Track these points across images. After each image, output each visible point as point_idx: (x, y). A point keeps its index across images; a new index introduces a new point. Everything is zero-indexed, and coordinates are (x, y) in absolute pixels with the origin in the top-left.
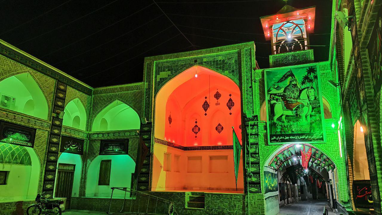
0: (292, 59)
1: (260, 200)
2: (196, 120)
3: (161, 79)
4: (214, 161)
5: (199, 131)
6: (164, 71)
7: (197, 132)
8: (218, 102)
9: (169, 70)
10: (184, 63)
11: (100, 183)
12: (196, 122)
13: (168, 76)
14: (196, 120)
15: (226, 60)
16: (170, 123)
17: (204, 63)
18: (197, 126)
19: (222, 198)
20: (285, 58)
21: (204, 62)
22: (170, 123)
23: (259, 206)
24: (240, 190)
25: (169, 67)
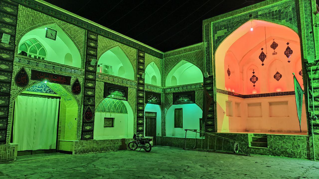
3: (218, 37)
4: (274, 107)
15: (282, 10)
16: (229, 75)
17: (259, 16)
18: (255, 76)
22: (229, 75)
25: (225, 25)
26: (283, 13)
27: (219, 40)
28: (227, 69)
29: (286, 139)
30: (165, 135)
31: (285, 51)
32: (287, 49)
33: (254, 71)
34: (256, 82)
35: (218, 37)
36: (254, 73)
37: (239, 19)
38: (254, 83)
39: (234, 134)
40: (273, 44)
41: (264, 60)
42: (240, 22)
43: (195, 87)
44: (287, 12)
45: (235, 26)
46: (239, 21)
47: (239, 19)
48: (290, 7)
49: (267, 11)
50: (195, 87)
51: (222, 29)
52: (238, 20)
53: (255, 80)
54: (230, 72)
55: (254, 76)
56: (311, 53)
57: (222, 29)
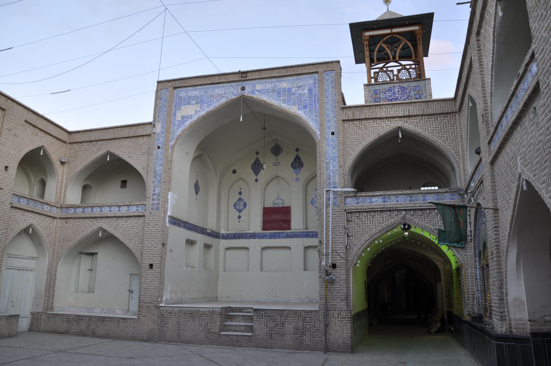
0: (398, 91)
1: (345, 318)
2: (240, 189)
3: (183, 117)
4: (267, 253)
5: (245, 208)
6: (189, 104)
7: (240, 210)
8: (277, 160)
9: (197, 103)
10: (224, 91)
11: (94, 293)
12: (240, 193)
13: (196, 113)
14: (240, 189)
15: (294, 89)
16: (197, 193)
17: (257, 92)
18: (243, 200)
19: (130, 233)
20: (388, 90)
21: (257, 91)
22: (197, 193)
23: (343, 329)
24: (83, 326)
25: (197, 97)
26: (294, 94)
27: (185, 123)
28: (195, 181)
29: (285, 317)
30: (52, 309)
31: (293, 162)
32: (295, 159)
33: (238, 220)
34: (242, 210)
35: (183, 117)
36: (239, 217)
37: (222, 91)
38: (240, 212)
39: (194, 309)
40: (276, 148)
41: (259, 172)
42: (224, 97)
43: (136, 209)
44: (300, 94)
45: (215, 103)
46: (222, 94)
47: (222, 91)
48: (306, 87)
49: (270, 86)
50: (136, 209)
51: (192, 103)
52: (221, 93)
53: (241, 208)
54: (198, 186)
55: (240, 211)
56: (331, 167)
57: (192, 103)
